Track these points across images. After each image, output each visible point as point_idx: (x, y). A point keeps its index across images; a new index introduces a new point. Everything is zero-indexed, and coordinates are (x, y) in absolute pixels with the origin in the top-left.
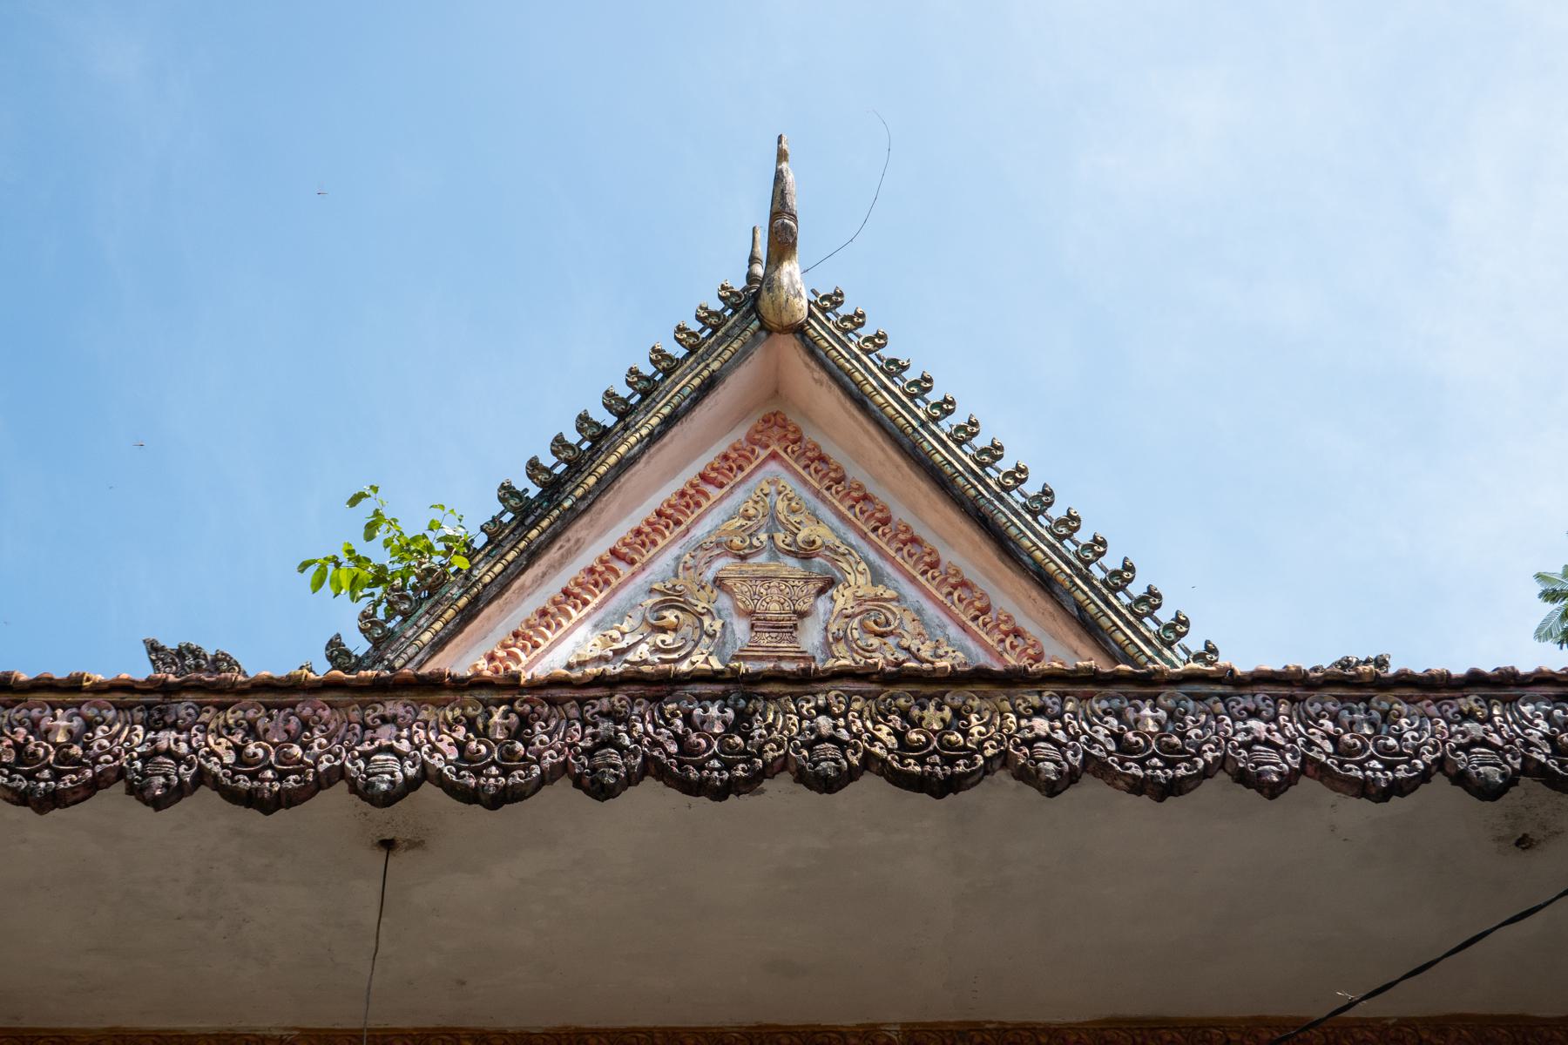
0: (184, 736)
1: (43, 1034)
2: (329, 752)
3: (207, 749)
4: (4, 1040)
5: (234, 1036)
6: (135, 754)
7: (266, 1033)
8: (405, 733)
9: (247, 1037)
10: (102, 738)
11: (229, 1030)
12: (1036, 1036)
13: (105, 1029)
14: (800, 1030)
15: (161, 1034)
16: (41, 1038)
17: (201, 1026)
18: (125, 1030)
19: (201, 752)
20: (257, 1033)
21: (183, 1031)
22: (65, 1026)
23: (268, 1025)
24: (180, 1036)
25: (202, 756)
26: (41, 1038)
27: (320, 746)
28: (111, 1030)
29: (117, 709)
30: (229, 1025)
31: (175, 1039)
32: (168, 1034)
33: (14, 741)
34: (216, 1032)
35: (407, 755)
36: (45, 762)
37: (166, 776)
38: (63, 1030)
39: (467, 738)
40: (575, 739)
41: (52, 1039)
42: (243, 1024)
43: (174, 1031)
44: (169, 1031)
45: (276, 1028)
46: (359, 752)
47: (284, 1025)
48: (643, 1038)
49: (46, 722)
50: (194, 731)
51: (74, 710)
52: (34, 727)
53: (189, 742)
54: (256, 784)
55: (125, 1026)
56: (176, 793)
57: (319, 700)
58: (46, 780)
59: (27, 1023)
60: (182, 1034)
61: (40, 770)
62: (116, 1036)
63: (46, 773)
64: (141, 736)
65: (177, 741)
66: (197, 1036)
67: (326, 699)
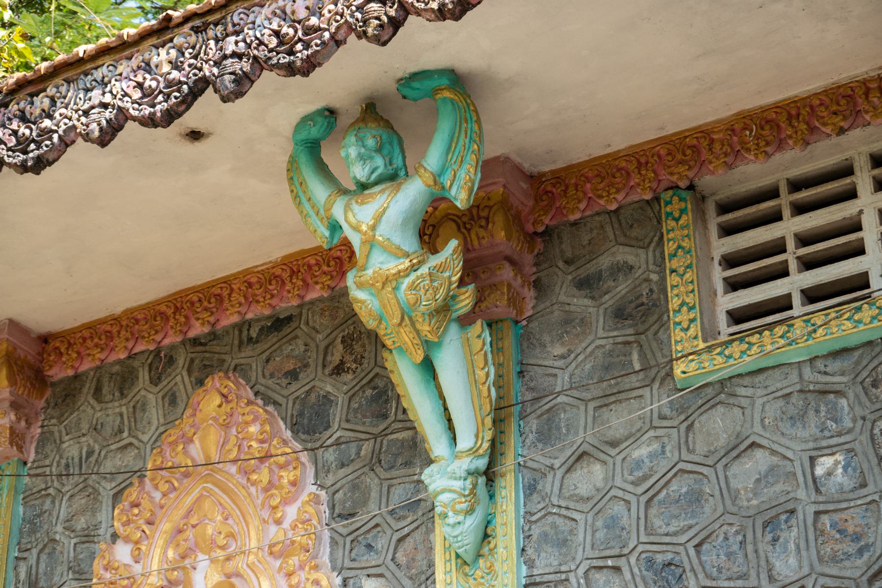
0: (241, 37)
1: (687, 134)
2: (337, 13)
3: (123, 93)
4: (659, 148)
5: (839, 87)
6: (354, 8)
7: (865, 76)
8: (108, 89)
9: (851, 85)
10: (190, 58)
11: (833, 84)
12: (709, 135)
13: (734, 115)
14: (646, 148)
15: (780, 105)
16: (686, 137)
17: (809, 88)
18: (749, 111)
19: (254, 45)
20: (857, 79)
21: (796, 97)
22: (701, 122)
23: (864, 69)
24: (795, 102)
25: (255, 48)
26: (686, 137)
27: (190, 66)
28: (738, 114)
29: (196, 32)
30: (831, 80)
31: (792, 105)
32: (786, 102)
33: (272, 30)
34: (824, 89)
35: (243, 54)
36: (296, 38)
37: (377, 18)
38: (700, 126)
39: (280, 26)
40: (79, 105)
41: (695, 136)
42: (843, 76)
43: (790, 99)
44: (785, 100)
45: (872, 70)
46: (355, 6)
47: (878, 66)
48: (856, 87)
49: (155, 60)
50: (246, 30)
51: (170, 45)
52: (23, 118)
53: (244, 41)
54: (292, 58)
55: (747, 108)
56: (243, 82)
57: (59, 80)
58: (300, 51)
59: (671, 130)
60: (796, 99)
61: (29, 145)
62: (744, 117)
63: (299, 47)
64: (214, 48)
65: (236, 43)
66: (809, 97)
67: (151, 43)
